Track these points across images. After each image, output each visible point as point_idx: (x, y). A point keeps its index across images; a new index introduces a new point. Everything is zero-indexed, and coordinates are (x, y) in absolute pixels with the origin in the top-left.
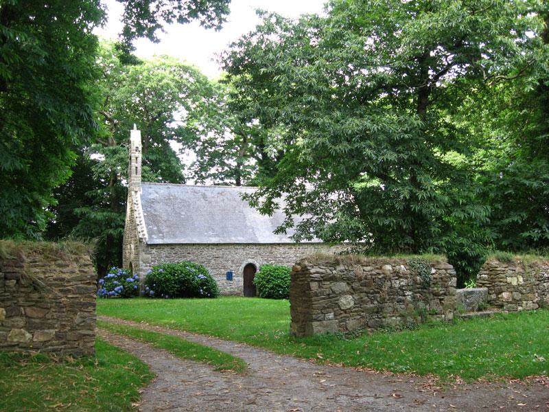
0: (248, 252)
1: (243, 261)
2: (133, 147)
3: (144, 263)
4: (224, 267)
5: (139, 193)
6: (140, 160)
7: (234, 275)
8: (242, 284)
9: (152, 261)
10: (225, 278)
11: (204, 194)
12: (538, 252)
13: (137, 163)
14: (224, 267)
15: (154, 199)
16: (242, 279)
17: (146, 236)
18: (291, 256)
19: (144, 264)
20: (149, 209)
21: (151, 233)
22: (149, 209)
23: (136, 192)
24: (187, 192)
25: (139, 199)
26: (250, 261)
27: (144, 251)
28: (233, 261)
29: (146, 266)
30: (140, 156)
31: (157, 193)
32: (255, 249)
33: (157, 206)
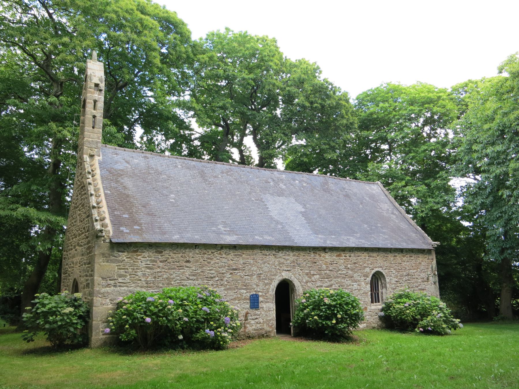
0: (282, 260)
1: (275, 275)
2: (91, 84)
3: (103, 278)
4: (246, 286)
5: (97, 158)
6: (101, 105)
7: (261, 299)
8: (275, 315)
9: (120, 276)
10: (248, 306)
11: (203, 171)
12: (280, 365)
13: (95, 108)
14: (246, 286)
15: (122, 170)
16: (272, 306)
17: (110, 228)
18: (341, 268)
19: (104, 282)
20: (113, 185)
21: (117, 222)
22: (113, 185)
23: (92, 156)
24: (176, 167)
25: (97, 166)
26: (285, 275)
27: (103, 254)
28: (259, 275)
29: (108, 285)
30: (101, 98)
31: (128, 162)
32: (291, 257)
33: (128, 182)
